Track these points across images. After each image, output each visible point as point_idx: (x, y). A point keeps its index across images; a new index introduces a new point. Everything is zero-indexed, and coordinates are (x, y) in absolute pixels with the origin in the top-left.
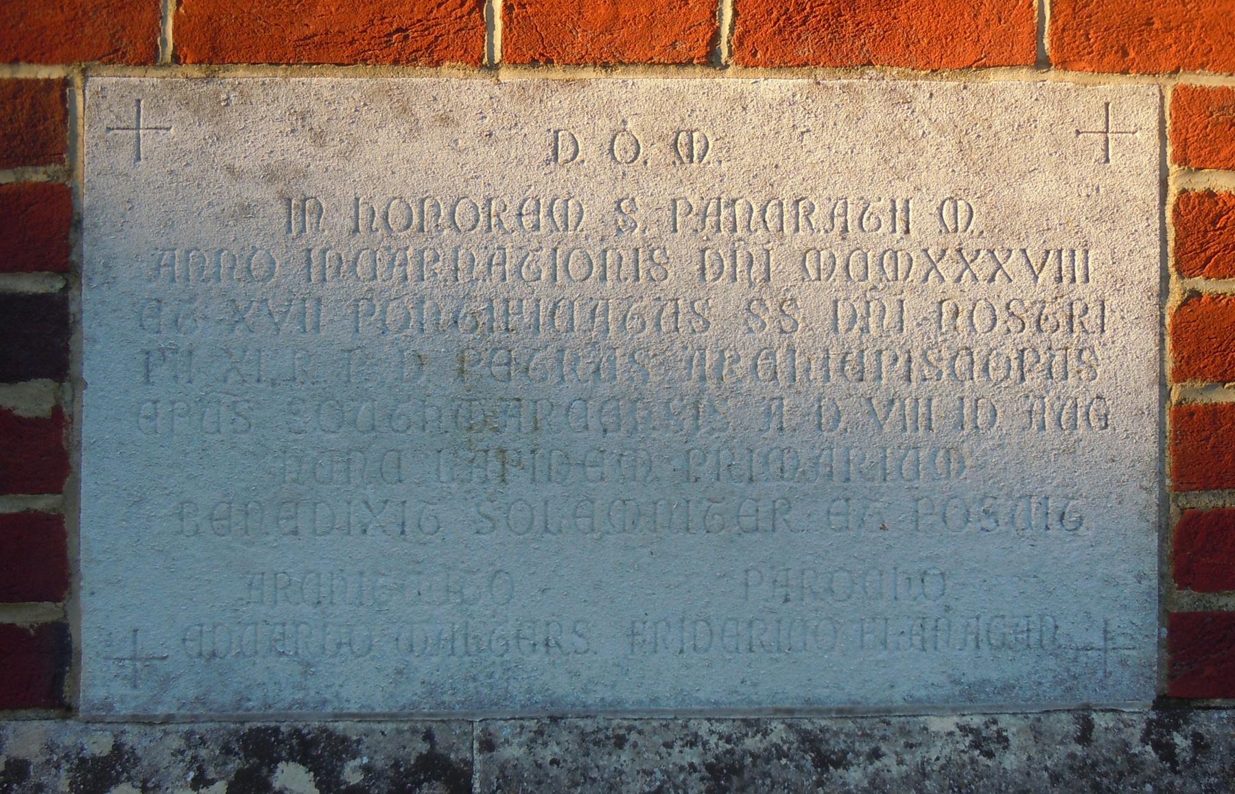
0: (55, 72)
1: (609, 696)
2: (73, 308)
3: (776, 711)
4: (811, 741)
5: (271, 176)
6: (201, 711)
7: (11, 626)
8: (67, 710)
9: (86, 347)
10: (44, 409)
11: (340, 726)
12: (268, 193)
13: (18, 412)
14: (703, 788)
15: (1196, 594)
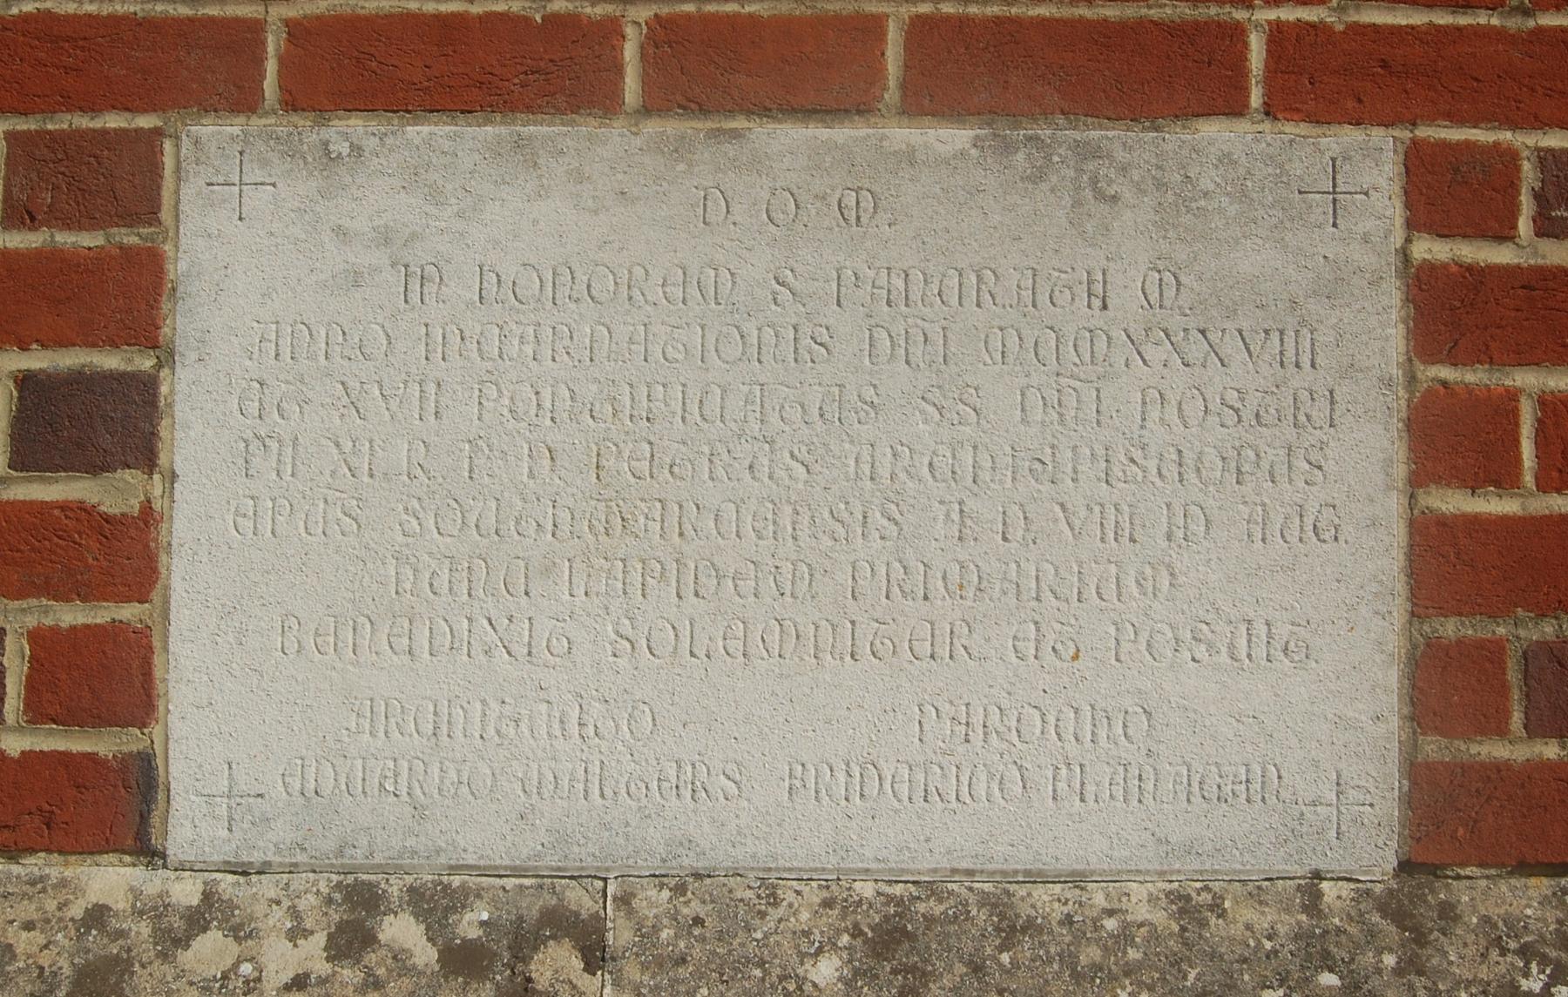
0: (145, 122)
1: (762, 850)
2: (164, 389)
3: (954, 871)
4: (995, 906)
5: (385, 238)
6: (301, 858)
7: (92, 757)
8: (148, 852)
9: (179, 434)
10: (134, 506)
11: (456, 881)
12: (379, 257)
13: (103, 508)
14: (28, 989)
15: (1444, 741)
